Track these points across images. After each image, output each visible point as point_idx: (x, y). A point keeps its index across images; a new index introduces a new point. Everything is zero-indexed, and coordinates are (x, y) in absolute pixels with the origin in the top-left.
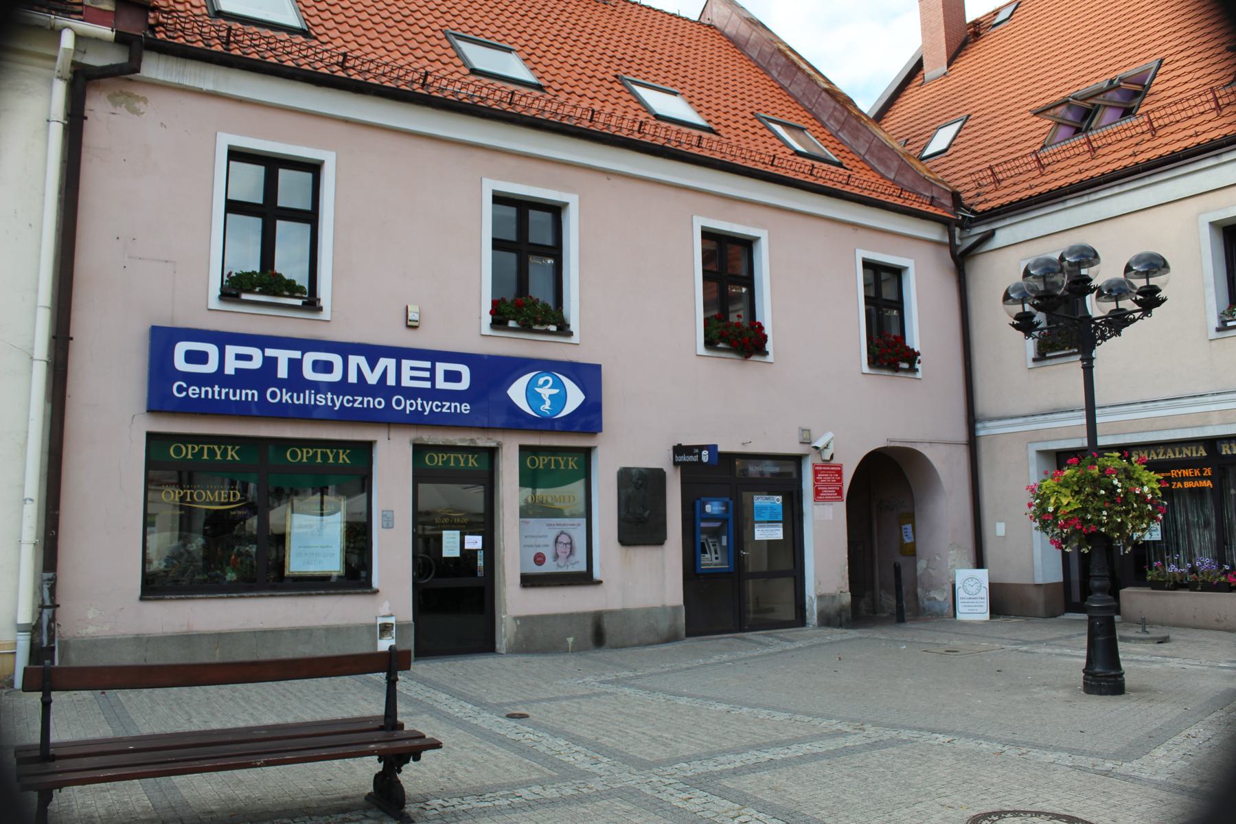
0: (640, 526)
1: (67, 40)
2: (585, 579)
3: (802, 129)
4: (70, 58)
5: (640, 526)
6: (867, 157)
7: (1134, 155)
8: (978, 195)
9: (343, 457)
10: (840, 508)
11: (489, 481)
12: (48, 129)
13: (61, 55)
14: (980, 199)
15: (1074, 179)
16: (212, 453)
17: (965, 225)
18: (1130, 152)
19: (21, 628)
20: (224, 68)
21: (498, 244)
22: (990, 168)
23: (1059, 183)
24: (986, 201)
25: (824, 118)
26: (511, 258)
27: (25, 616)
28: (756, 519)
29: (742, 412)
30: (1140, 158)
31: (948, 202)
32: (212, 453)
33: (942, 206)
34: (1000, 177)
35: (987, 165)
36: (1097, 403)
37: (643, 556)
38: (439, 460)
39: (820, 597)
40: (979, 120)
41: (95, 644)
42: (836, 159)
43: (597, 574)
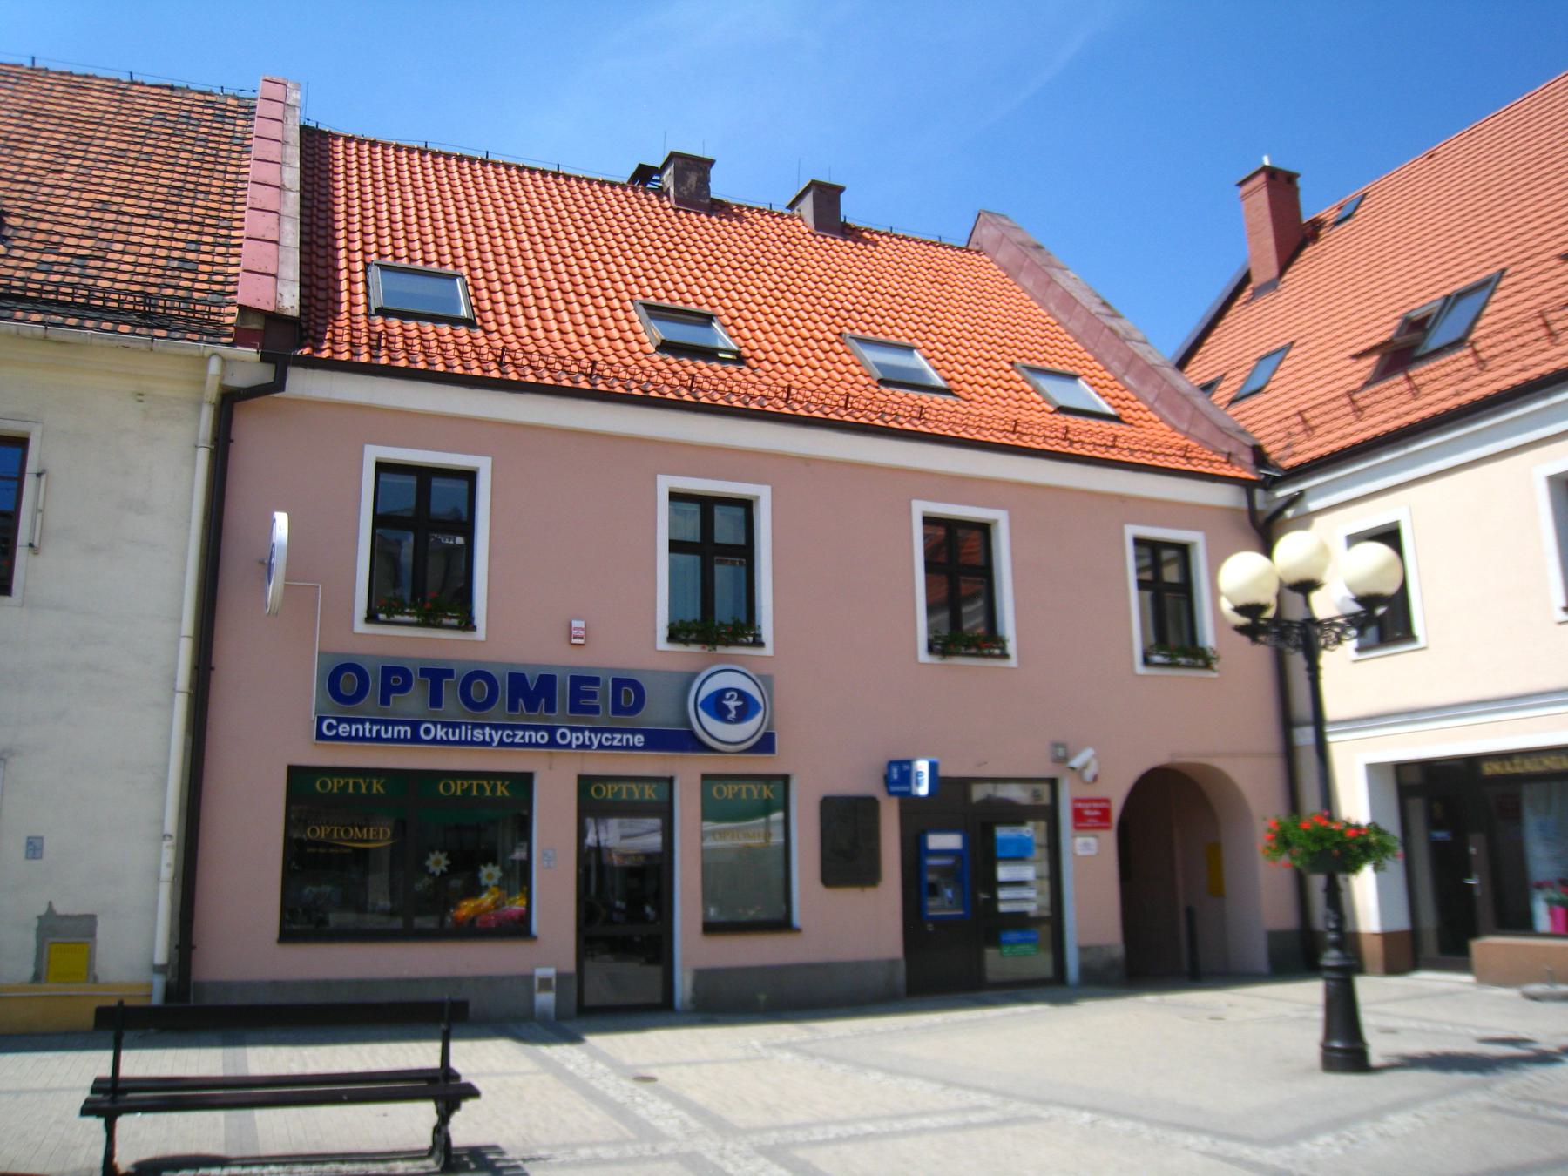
0: (847, 860)
1: (214, 366)
2: (782, 924)
3: (1074, 377)
4: (216, 382)
5: (847, 860)
6: (1157, 405)
7: (1457, 394)
8: (1288, 447)
9: (501, 790)
10: (1109, 837)
11: (665, 810)
12: (195, 455)
13: (209, 379)
14: (1288, 452)
15: (1451, 403)
16: (481, 788)
17: (1270, 484)
18: (1451, 390)
19: (158, 969)
20: (209, 733)
21: (675, 546)
22: (1300, 413)
23: (1433, 409)
24: (1294, 455)
25: (1108, 359)
26: (692, 561)
27: (161, 957)
28: (1000, 853)
29: (962, 727)
30: (1464, 399)
31: (1247, 457)
32: (481, 788)
33: (1241, 463)
34: (1313, 423)
35: (1295, 411)
36: (1332, 710)
37: (849, 899)
38: (729, 790)
39: (1083, 950)
40: (1304, 348)
41: (227, 986)
42: (1110, 411)
43: (797, 919)
